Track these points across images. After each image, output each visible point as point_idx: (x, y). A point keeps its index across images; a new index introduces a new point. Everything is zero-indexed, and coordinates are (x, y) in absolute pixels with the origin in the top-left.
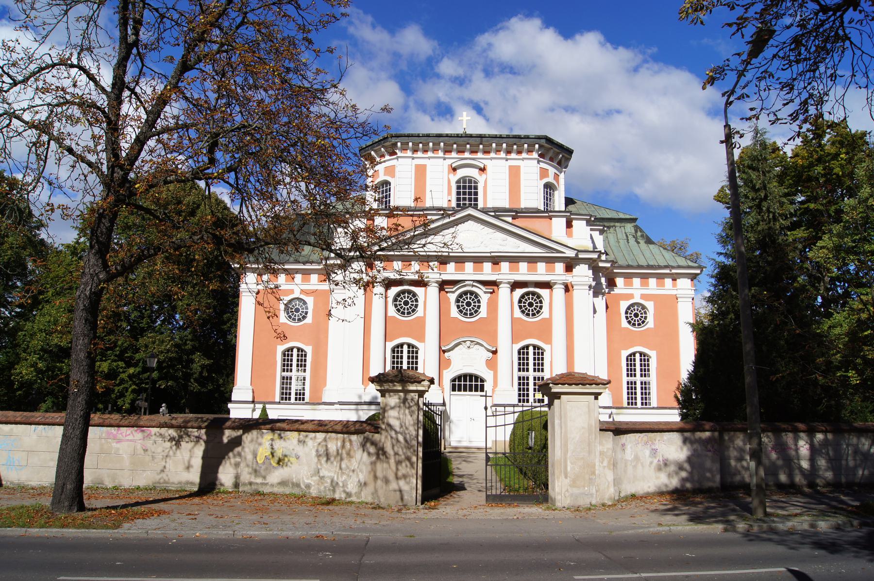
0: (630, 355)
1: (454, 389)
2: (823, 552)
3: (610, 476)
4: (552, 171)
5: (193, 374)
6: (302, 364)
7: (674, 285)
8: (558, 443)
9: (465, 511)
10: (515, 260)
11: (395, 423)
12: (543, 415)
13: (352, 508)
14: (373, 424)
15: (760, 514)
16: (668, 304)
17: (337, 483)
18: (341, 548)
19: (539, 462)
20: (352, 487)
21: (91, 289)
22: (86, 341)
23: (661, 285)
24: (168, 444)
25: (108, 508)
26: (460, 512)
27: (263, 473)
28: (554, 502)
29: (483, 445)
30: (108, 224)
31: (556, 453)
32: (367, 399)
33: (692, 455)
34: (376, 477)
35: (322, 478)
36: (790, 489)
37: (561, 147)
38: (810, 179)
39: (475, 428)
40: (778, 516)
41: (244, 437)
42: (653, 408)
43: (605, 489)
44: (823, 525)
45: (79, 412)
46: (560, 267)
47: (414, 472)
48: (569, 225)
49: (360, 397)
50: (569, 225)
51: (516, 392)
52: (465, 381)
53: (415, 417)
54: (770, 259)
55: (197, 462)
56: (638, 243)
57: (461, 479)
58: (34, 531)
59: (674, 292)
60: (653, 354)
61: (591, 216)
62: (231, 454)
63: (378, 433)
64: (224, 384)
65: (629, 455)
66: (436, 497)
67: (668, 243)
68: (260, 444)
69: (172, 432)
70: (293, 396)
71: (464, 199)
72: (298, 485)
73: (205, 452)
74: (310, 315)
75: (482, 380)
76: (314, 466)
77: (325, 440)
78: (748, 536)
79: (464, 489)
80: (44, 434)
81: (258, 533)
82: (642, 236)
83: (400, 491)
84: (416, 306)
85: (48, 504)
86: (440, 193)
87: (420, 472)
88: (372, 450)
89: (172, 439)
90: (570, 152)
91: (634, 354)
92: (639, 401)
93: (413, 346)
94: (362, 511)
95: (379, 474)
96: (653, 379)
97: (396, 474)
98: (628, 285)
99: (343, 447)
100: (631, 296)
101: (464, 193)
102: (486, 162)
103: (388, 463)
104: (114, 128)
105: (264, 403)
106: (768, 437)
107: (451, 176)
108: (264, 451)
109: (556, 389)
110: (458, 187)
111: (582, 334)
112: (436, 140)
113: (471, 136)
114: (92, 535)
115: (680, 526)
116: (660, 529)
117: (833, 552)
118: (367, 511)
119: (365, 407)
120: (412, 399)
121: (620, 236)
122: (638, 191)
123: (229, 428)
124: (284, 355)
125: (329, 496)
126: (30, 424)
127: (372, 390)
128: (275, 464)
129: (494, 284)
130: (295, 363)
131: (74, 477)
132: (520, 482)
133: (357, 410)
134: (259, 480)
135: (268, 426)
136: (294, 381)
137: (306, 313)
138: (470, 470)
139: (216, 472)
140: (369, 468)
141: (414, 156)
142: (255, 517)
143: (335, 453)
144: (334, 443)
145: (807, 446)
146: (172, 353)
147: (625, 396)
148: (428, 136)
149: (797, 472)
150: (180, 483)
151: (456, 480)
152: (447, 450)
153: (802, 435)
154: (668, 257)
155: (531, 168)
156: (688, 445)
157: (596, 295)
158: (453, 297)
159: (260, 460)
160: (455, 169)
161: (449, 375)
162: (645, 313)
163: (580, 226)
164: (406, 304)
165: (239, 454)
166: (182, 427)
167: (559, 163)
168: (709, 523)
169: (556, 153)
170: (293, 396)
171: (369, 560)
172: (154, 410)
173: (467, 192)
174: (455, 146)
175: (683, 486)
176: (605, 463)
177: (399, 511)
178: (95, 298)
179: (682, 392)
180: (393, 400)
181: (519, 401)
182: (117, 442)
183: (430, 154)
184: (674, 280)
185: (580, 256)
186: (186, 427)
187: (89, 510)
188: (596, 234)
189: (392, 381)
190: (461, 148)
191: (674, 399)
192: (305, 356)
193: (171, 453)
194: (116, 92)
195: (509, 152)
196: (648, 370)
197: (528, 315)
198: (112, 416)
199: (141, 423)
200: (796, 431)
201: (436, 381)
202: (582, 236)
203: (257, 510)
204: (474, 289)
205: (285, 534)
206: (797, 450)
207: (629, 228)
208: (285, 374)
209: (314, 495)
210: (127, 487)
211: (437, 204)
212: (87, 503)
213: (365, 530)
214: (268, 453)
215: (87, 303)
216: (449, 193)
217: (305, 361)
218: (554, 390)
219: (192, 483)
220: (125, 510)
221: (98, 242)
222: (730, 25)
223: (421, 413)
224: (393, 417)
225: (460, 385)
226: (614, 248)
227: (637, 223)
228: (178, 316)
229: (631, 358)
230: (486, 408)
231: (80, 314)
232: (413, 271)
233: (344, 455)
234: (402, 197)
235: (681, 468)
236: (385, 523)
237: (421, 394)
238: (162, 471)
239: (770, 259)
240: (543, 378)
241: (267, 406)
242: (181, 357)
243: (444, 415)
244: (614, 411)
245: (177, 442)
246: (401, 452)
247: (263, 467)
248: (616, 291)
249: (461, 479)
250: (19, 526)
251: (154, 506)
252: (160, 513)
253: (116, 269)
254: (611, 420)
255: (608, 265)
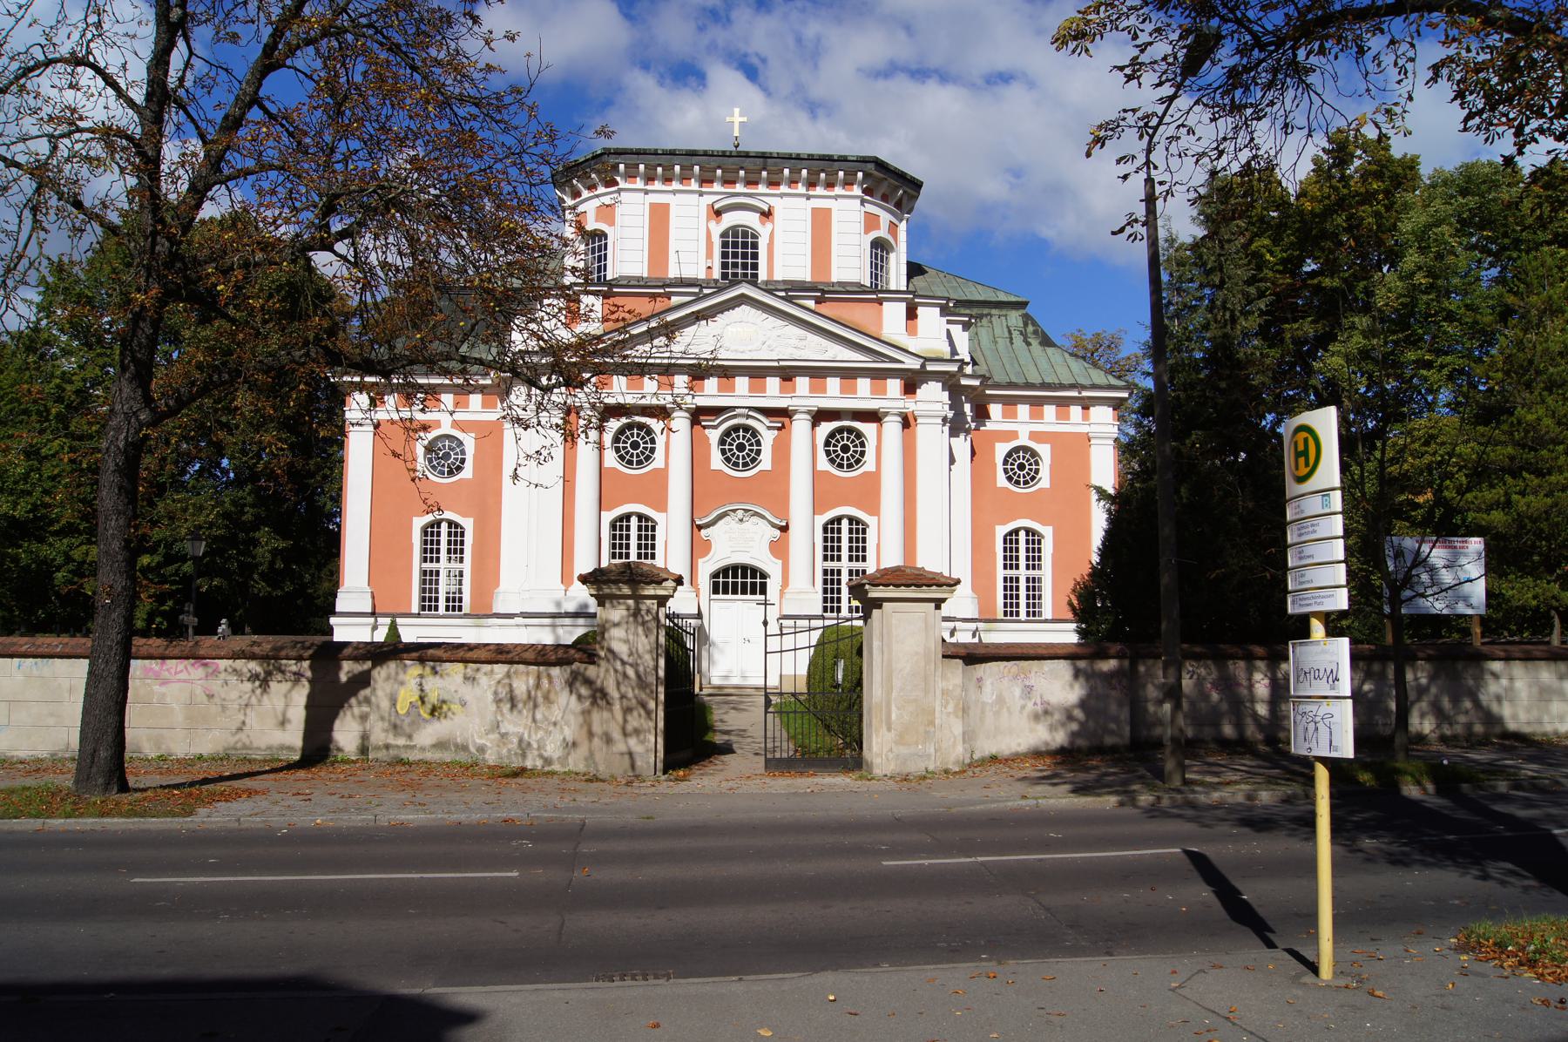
0: (1010, 534)
1: (716, 591)
2: (1246, 830)
3: (957, 728)
4: (885, 217)
5: (257, 566)
6: (456, 549)
7: (1086, 418)
8: (877, 677)
9: (731, 784)
10: (818, 373)
11: (621, 648)
12: (856, 634)
13: (556, 780)
14: (587, 650)
15: (1177, 783)
16: (1074, 449)
17: (529, 744)
18: (544, 834)
19: (850, 707)
20: (553, 749)
21: (126, 438)
22: (121, 522)
23: (1063, 417)
24: (248, 686)
25: (168, 786)
26: (724, 784)
27: (408, 730)
28: (870, 767)
29: (761, 682)
30: (149, 331)
31: (875, 692)
32: (570, 607)
33: (1089, 696)
34: (591, 735)
35: (504, 736)
36: (1239, 746)
37: (901, 177)
38: (1324, 235)
39: (747, 653)
40: (1202, 784)
41: (375, 673)
42: (1046, 621)
43: (948, 746)
44: (1265, 797)
45: (114, 635)
46: (894, 386)
47: (652, 724)
48: (911, 314)
49: (558, 604)
50: (911, 314)
51: (820, 596)
52: (735, 576)
53: (653, 638)
54: (1223, 385)
55: (298, 714)
56: (1029, 344)
57: (726, 737)
58: (57, 823)
59: (1084, 429)
60: (1047, 532)
61: (948, 299)
62: (353, 701)
63: (593, 663)
64: (312, 583)
65: (988, 694)
66: (687, 764)
67: (1089, 336)
68: (402, 683)
69: (254, 666)
70: (442, 604)
71: (735, 265)
72: (465, 748)
73: (310, 697)
74: (469, 465)
75: (764, 576)
76: (490, 717)
77: (508, 675)
78: (1153, 812)
79: (732, 751)
80: (35, 672)
81: (412, 818)
82: (1035, 332)
83: (630, 754)
84: (653, 450)
85: (70, 784)
86: (693, 254)
87: (661, 724)
88: (584, 691)
89: (254, 677)
90: (916, 185)
91: (1016, 531)
92: (1023, 609)
93: (647, 519)
94: (572, 785)
95: (597, 729)
96: (1046, 573)
97: (624, 729)
98: (1010, 415)
99: (538, 686)
100: (1013, 435)
101: (735, 255)
102: (772, 201)
103: (611, 711)
104: (149, 165)
105: (394, 616)
106: (1206, 667)
107: (712, 224)
108: (407, 695)
109: (875, 593)
110: (725, 245)
111: (930, 501)
112: (687, 161)
113: (747, 155)
114: (152, 827)
115: (1059, 799)
116: (1023, 802)
117: (1259, 831)
118: (578, 785)
119: (567, 621)
120: (648, 611)
121: (998, 331)
122: (1047, 232)
123: (348, 658)
124: (426, 534)
125: (516, 763)
126: (11, 656)
127: (581, 594)
128: (426, 716)
129: (784, 413)
130: (444, 547)
131: (110, 739)
132: (820, 740)
133: (554, 626)
134: (401, 741)
135: (415, 655)
136: (443, 578)
137: (463, 461)
138: (743, 723)
139: (331, 729)
140: (581, 719)
141: (649, 187)
142: (402, 796)
143: (525, 696)
144: (523, 680)
145: (1266, 681)
146: (219, 528)
147: (1000, 601)
148: (672, 153)
149: (1249, 721)
150: (269, 748)
151: (719, 739)
152: (705, 691)
153: (1261, 664)
154: (1078, 370)
155: (849, 211)
156: (1082, 679)
157: (954, 433)
158: (714, 436)
159: (402, 708)
160: (718, 213)
161: (707, 567)
162: (1037, 463)
163: (929, 316)
164: (635, 444)
165: (367, 701)
166: (271, 659)
167: (898, 205)
168: (1099, 795)
169: (891, 185)
170: (442, 604)
171: (585, 848)
172: (207, 628)
173: (740, 252)
174: (719, 172)
175: (1072, 743)
176: (950, 708)
177: (629, 784)
178: (135, 450)
179: (1079, 598)
180: (617, 613)
181: (825, 609)
182: (162, 684)
183: (675, 185)
184: (1085, 408)
185: (929, 368)
186: (277, 658)
187: (136, 790)
188: (957, 330)
189: (616, 582)
190: (730, 176)
191: (1067, 608)
192: (462, 534)
193: (254, 700)
194: (155, 107)
195: (811, 184)
196: (1040, 558)
197: (840, 466)
198: (150, 641)
199: (202, 652)
200: (1250, 658)
201: (686, 580)
202: (933, 333)
203: (404, 787)
204: (750, 422)
205: (455, 817)
206: (1251, 686)
207: (1015, 318)
208: (428, 566)
209: (491, 763)
210: (181, 756)
211: (689, 272)
212: (131, 783)
213: (578, 810)
214: (415, 698)
215: (120, 460)
216: (709, 255)
217: (462, 543)
218: (872, 595)
219: (290, 748)
220: (193, 790)
221: (134, 359)
222: (1121, 69)
223: (662, 633)
224: (618, 640)
225: (726, 584)
226: (987, 353)
227: (1028, 310)
228: (225, 462)
229: (1011, 538)
230: (765, 623)
231: (109, 478)
232: (650, 390)
233: (540, 700)
234: (627, 258)
235: (1070, 718)
236: (607, 800)
237: (662, 601)
238: (240, 729)
239: (1223, 385)
240: (864, 572)
241: (399, 621)
242: (233, 537)
243: (701, 635)
244: (981, 625)
245: (264, 682)
246: (630, 695)
247: (407, 720)
248: (989, 426)
249: (726, 737)
250: (30, 816)
251: (237, 784)
252: (250, 793)
253: (167, 405)
254: (976, 640)
255: (976, 383)
